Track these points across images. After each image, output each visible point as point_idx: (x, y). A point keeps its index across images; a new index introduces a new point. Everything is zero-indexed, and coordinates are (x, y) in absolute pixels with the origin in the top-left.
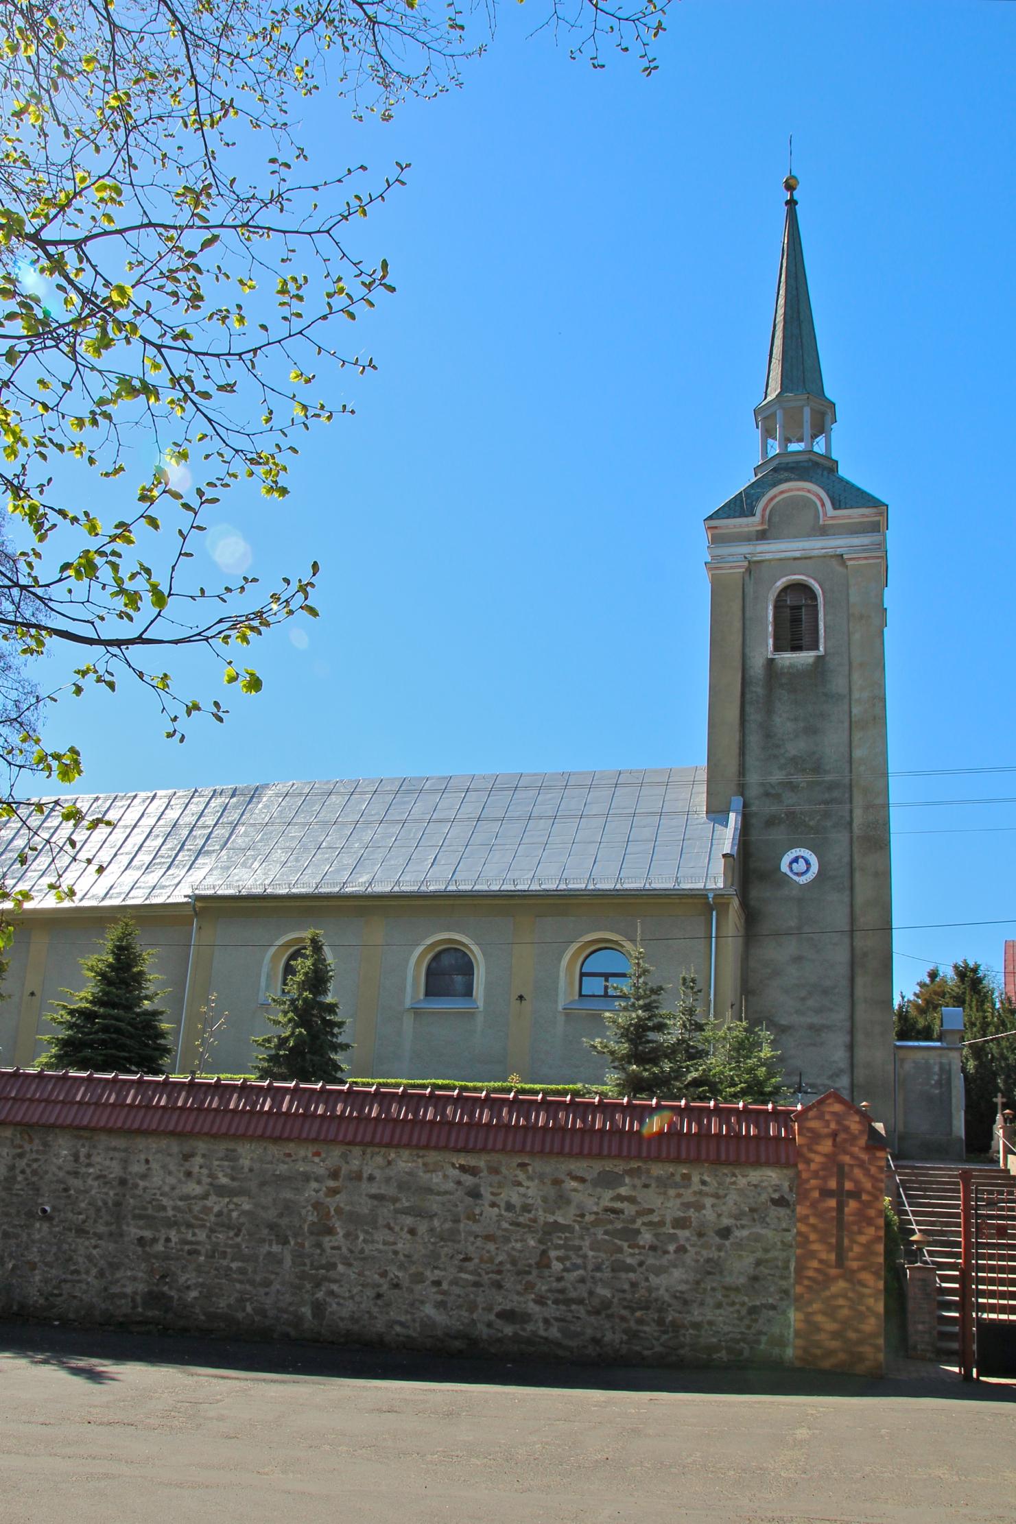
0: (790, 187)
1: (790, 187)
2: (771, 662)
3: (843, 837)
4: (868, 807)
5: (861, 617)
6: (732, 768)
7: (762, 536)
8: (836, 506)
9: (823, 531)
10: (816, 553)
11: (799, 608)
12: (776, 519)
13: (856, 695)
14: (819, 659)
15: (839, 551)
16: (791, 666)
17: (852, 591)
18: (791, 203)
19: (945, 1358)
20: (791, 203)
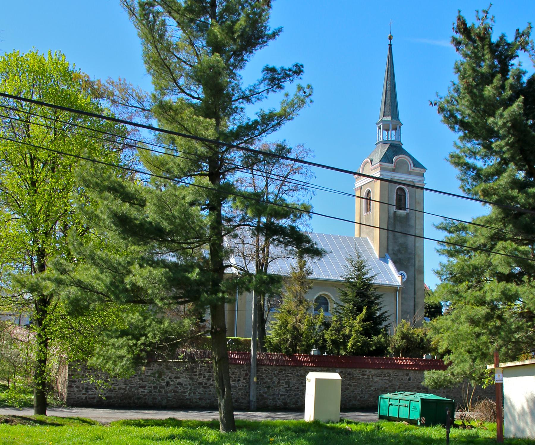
0: (390, 38)
1: (390, 38)
2: (395, 212)
3: (413, 269)
4: (419, 261)
5: (483, 236)
6: (385, 245)
7: (394, 171)
8: (414, 167)
9: (410, 173)
10: (408, 180)
11: (401, 196)
12: (397, 166)
13: (417, 227)
14: (407, 213)
15: (414, 181)
16: (400, 215)
17: (417, 194)
18: (390, 45)
19: (320, 369)
20: (390, 45)
